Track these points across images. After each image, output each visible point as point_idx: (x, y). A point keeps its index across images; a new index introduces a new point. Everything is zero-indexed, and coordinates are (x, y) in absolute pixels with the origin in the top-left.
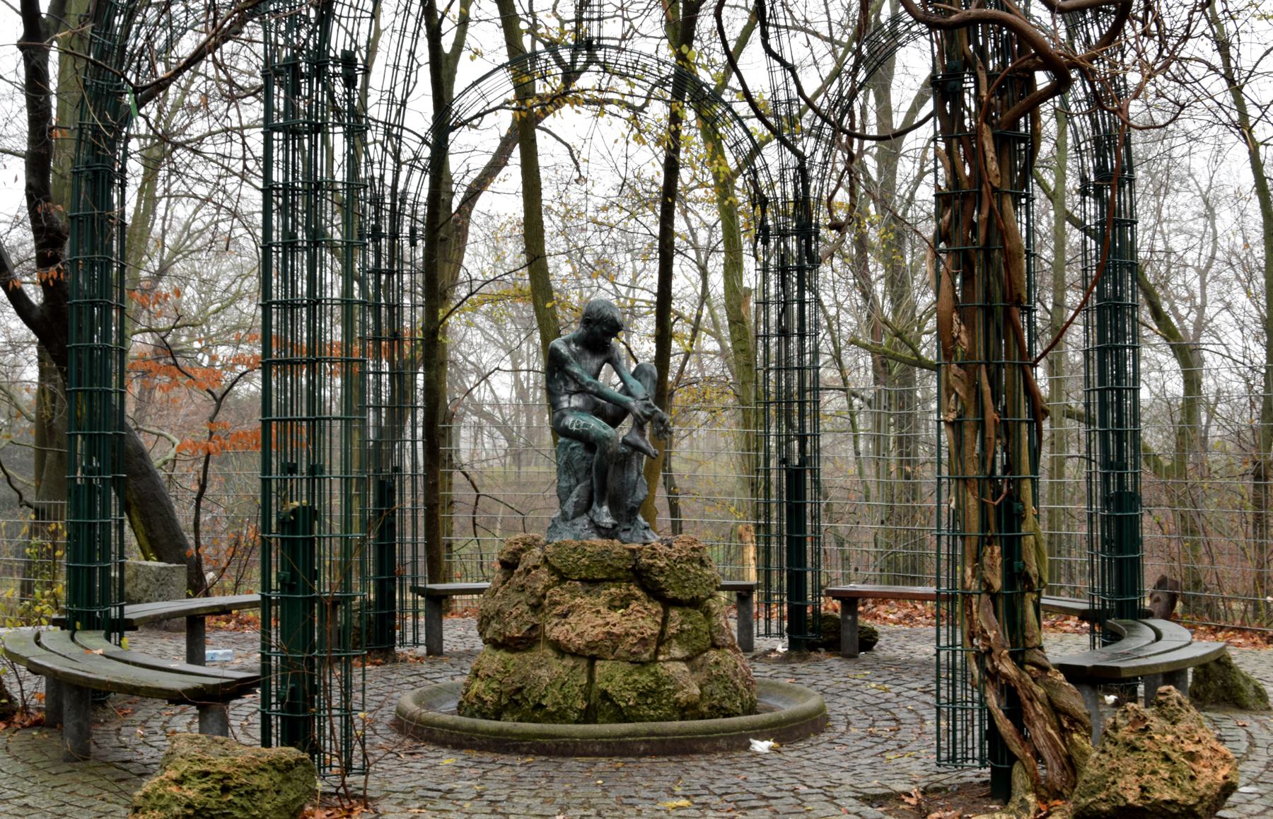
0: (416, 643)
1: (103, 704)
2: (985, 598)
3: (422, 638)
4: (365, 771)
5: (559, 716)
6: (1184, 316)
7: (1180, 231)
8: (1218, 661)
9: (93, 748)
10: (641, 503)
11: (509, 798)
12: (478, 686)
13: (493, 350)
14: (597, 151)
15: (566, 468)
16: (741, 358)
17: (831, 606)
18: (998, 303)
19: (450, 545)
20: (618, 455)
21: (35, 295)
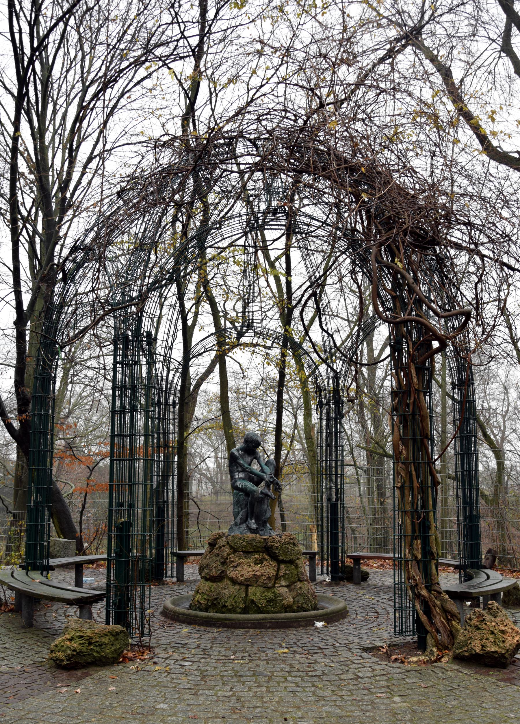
0: (172, 577)
1: (39, 602)
2: (414, 562)
3: (175, 573)
4: (150, 636)
5: (233, 611)
6: (495, 434)
7: (494, 399)
8: (514, 588)
9: (34, 622)
10: (269, 518)
11: (211, 648)
12: (198, 597)
13: (207, 447)
14: (251, 366)
15: (237, 503)
16: (311, 453)
17: (349, 562)
18: (418, 437)
19: (187, 532)
20: (259, 498)
21: (16, 425)
